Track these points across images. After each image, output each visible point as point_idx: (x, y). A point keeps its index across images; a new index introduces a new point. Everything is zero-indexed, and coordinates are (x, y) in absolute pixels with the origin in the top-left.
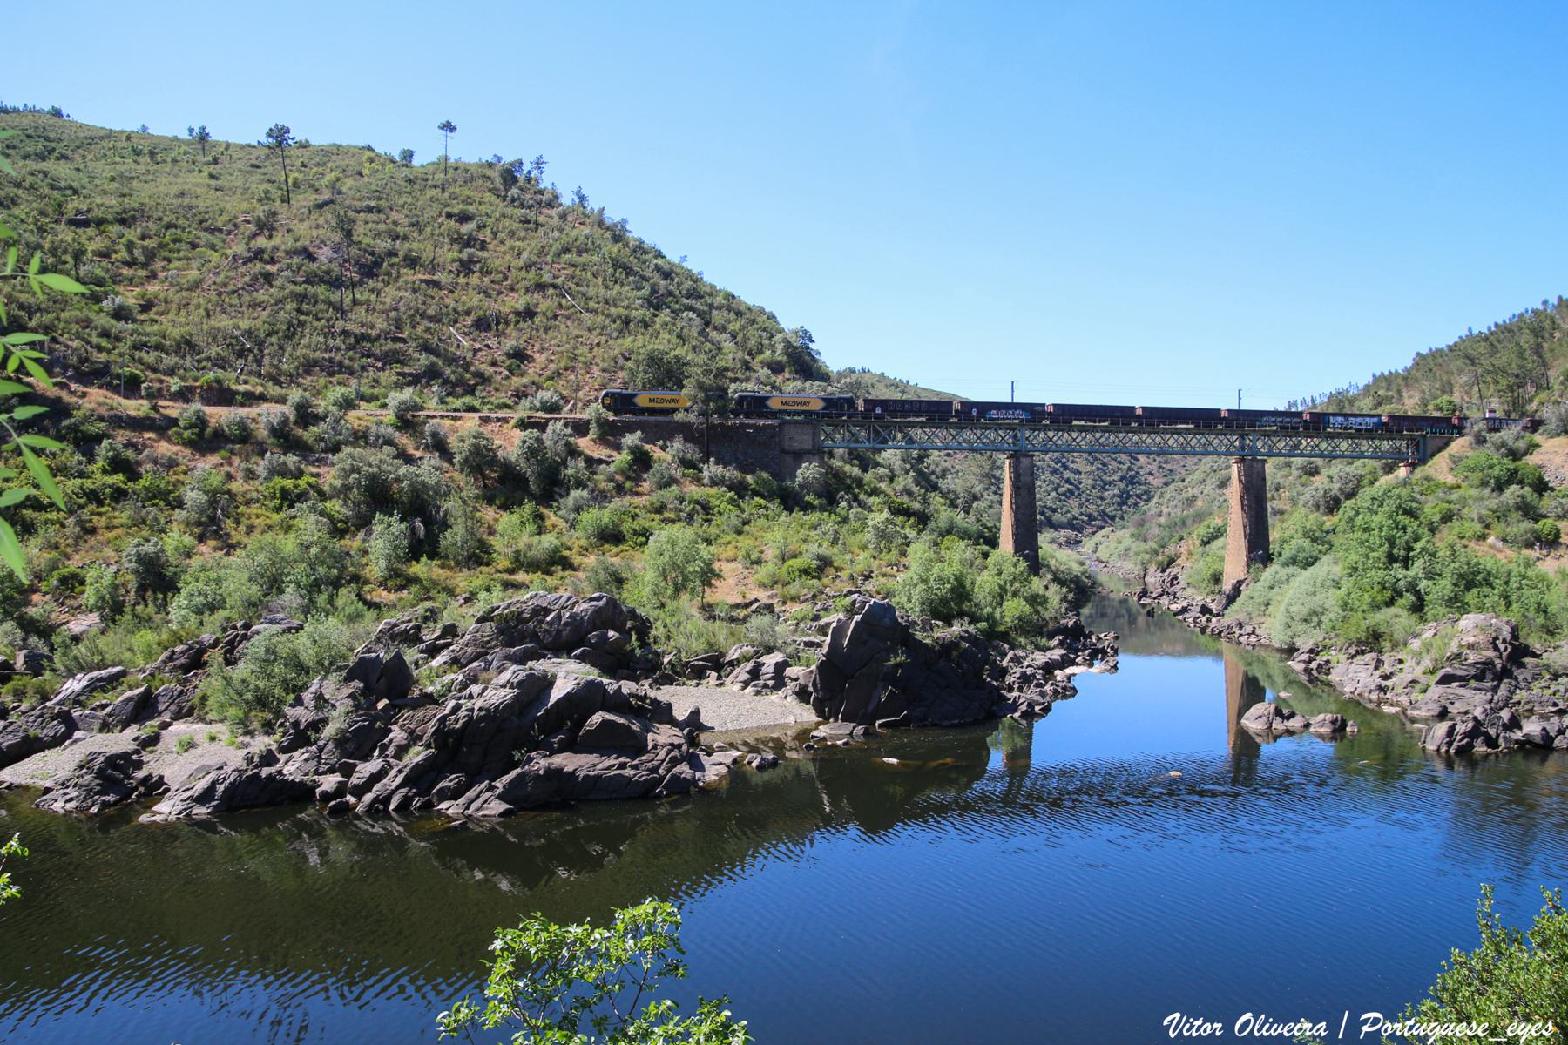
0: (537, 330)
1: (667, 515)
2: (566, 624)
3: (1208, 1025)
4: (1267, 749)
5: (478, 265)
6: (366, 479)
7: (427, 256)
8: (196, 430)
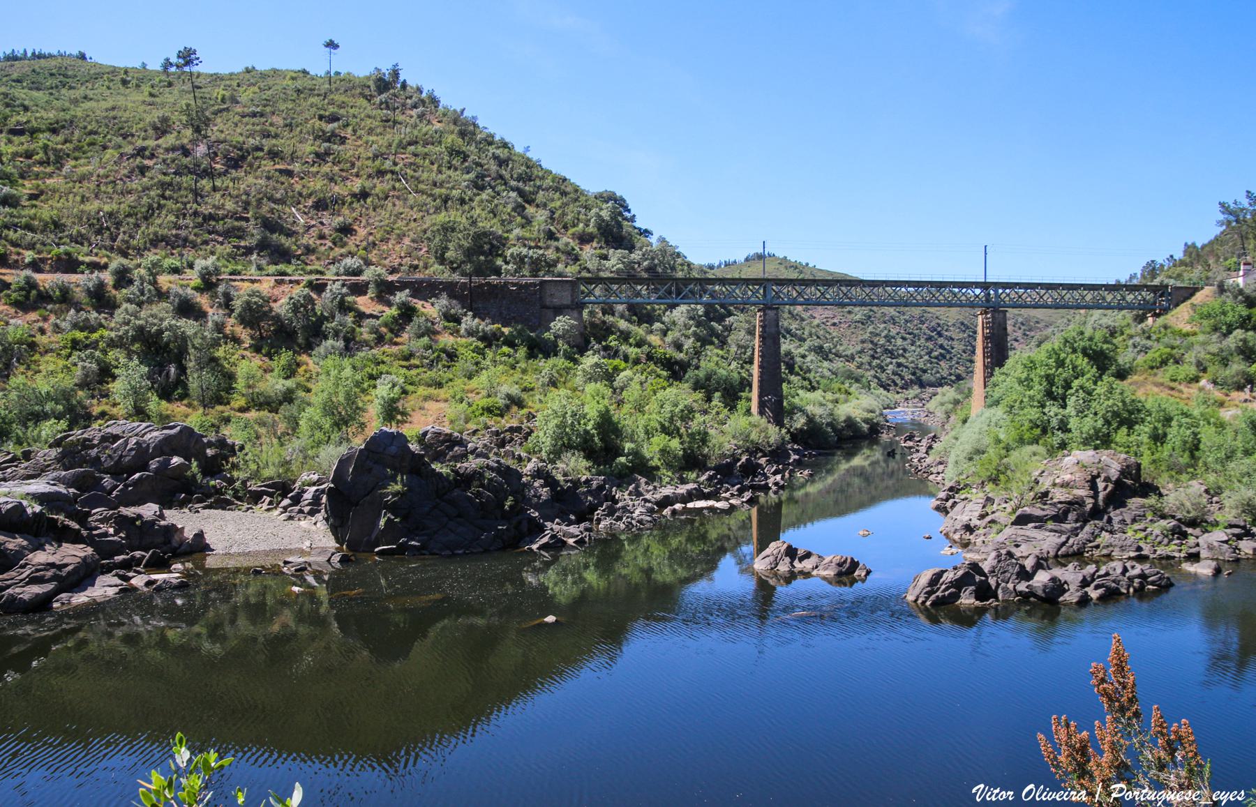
0: (367, 209)
1: (413, 361)
2: (131, 449)
3: (1004, 792)
4: (782, 590)
5: (332, 157)
6: (134, 329)
7: (287, 151)
8: (24, 293)
